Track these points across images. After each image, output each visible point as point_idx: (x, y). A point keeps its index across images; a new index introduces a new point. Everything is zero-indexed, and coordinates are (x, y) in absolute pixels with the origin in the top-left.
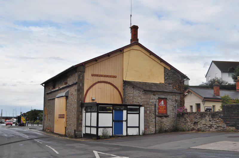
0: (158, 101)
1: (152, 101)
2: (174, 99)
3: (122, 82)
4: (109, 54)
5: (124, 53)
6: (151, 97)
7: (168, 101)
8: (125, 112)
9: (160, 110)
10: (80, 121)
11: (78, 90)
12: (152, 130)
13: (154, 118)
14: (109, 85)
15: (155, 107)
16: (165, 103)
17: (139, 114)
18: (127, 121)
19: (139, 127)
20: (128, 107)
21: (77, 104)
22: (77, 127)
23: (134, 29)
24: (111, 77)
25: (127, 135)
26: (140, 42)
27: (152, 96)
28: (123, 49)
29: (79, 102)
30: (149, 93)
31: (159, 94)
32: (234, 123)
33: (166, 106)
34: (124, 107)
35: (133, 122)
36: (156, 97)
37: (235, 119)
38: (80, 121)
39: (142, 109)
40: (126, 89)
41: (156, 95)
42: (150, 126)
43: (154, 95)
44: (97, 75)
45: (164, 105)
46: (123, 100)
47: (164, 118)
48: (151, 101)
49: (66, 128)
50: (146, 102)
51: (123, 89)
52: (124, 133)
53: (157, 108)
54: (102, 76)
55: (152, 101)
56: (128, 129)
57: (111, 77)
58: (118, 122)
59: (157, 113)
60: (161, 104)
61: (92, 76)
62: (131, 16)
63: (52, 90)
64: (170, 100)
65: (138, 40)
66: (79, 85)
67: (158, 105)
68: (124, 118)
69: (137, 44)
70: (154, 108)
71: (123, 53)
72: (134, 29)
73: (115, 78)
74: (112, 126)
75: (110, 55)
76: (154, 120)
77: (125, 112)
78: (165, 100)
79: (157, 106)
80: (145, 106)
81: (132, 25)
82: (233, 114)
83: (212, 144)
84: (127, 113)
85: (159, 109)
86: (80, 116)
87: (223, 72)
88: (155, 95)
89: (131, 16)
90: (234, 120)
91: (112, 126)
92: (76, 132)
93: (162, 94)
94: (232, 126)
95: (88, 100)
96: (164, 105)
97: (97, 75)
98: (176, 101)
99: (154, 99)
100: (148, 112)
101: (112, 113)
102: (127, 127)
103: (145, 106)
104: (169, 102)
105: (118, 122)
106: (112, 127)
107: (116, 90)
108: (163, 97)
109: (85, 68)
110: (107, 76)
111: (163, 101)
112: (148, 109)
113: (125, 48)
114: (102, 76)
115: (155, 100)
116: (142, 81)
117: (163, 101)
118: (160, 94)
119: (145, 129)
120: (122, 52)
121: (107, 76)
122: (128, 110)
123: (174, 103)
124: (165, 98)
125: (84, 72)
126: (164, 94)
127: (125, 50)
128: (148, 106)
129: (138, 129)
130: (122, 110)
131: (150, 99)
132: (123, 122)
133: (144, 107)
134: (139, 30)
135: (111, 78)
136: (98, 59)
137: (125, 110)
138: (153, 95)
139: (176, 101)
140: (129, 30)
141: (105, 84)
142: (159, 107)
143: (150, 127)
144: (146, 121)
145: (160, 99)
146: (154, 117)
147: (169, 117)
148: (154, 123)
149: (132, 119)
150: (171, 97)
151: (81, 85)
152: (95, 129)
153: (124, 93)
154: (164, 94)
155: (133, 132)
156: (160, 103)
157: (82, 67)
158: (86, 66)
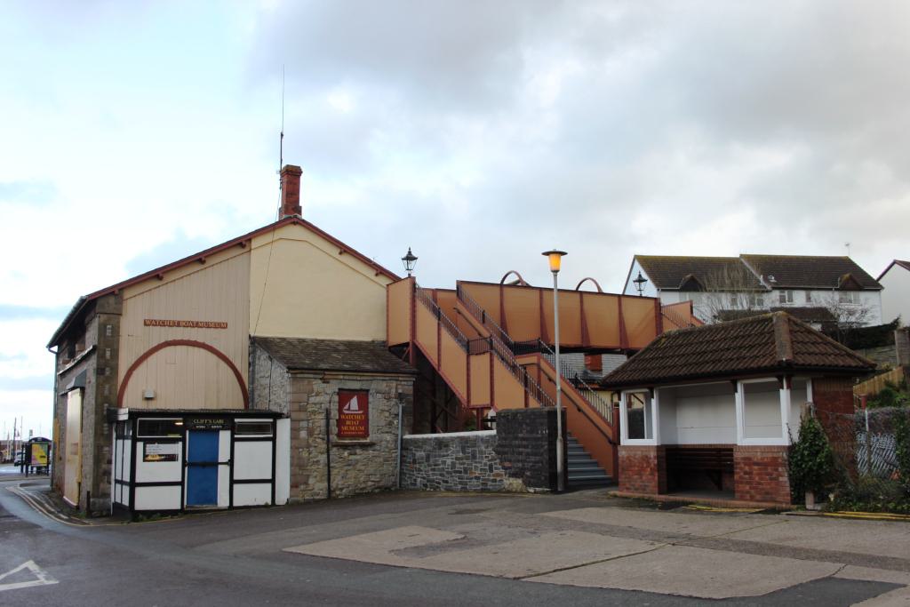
0: (336, 398)
1: (318, 399)
2: (394, 391)
3: (247, 342)
4: (160, 273)
5: (252, 251)
6: (315, 388)
7: (371, 399)
8: (225, 437)
9: (346, 428)
10: (104, 466)
11: (100, 371)
12: (316, 490)
13: (322, 453)
14: (202, 351)
15: (328, 418)
16: (364, 405)
17: (274, 440)
18: (231, 463)
19: (272, 481)
20: (236, 420)
21: (96, 413)
22: (96, 485)
23: (291, 176)
24: (207, 325)
25: (231, 506)
26: (306, 215)
27: (318, 385)
28: (250, 240)
29: (103, 404)
30: (306, 376)
31: (342, 377)
32: (520, 465)
33: (366, 413)
34: (221, 421)
35: (254, 468)
36: (334, 387)
37: (520, 453)
38: (104, 466)
39: (284, 427)
40: (257, 362)
41: (331, 381)
42: (308, 476)
43: (325, 381)
44: (163, 324)
45: (361, 412)
46: (247, 396)
47: (358, 451)
48: (312, 400)
49: (80, 484)
50: (297, 404)
51: (250, 364)
52: (223, 501)
53: (333, 422)
54: (178, 324)
55: (318, 399)
56: (236, 487)
57: (207, 325)
58: (201, 468)
59: (334, 438)
60: (349, 409)
61: (145, 324)
62: (282, 135)
63: (85, 368)
64: (379, 396)
65: (299, 210)
66: (102, 356)
67: (337, 412)
68: (223, 455)
69: (294, 223)
70: (323, 423)
71: (250, 251)
72: (291, 176)
73: (223, 330)
74: (180, 480)
75: (161, 275)
76: (323, 458)
77: (225, 437)
78: (363, 395)
79: (335, 415)
80: (294, 415)
81: (283, 165)
82: (516, 438)
83: (764, 586)
84: (233, 440)
85: (340, 422)
86: (106, 449)
87: (663, 290)
88: (328, 382)
89: (282, 135)
90: (520, 458)
91: (180, 480)
92: (91, 500)
93: (351, 377)
94: (514, 475)
95: (132, 401)
96: (361, 412)
97: (163, 324)
98: (400, 397)
99: (324, 393)
100: (303, 434)
101: (183, 440)
102: (233, 482)
103: (294, 415)
104: (376, 403)
105: (201, 468)
106: (181, 483)
107: (223, 364)
108: (356, 385)
109: (121, 303)
110: (197, 325)
111: (355, 397)
112: (304, 424)
113: (255, 237)
114: (178, 324)
115: (328, 398)
116: (313, 337)
117: (355, 397)
118: (346, 377)
119: (294, 486)
120: (247, 249)
121: (197, 325)
122: (234, 429)
123: (393, 402)
124: (361, 390)
125: (121, 315)
126: (359, 378)
127: (255, 243)
128: (303, 415)
129: (269, 486)
130: (217, 431)
131: (310, 393)
132: (220, 466)
133: (292, 421)
134: (303, 179)
135: (209, 329)
136: (206, 257)
137: (228, 429)
138: (320, 381)
139: (400, 397)
140: (276, 180)
141: (190, 348)
142: (343, 417)
143: (311, 481)
144: (298, 465)
145: (344, 396)
146: (325, 451)
147: (378, 448)
148: (322, 467)
149: (252, 457)
150: (383, 386)
151: (108, 354)
152: (126, 489)
153: (252, 374)
154: (359, 378)
155: (254, 496)
156: (346, 407)
157: (112, 300)
158: (125, 298)
